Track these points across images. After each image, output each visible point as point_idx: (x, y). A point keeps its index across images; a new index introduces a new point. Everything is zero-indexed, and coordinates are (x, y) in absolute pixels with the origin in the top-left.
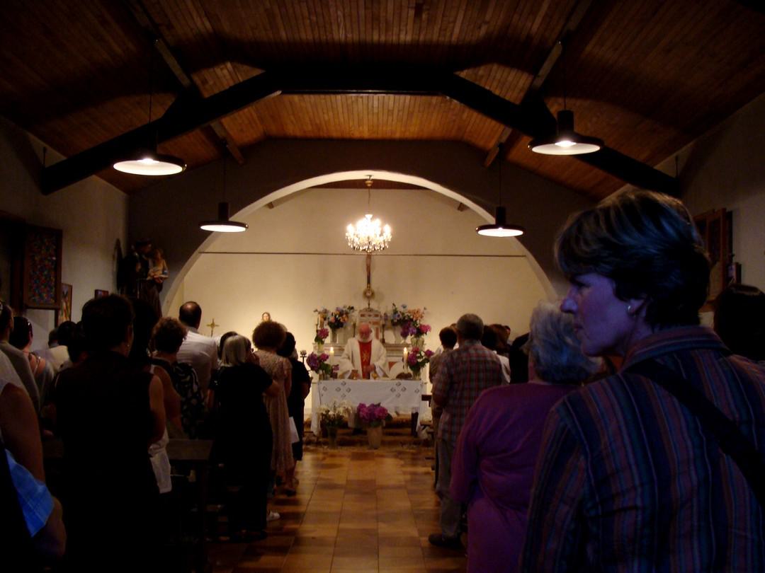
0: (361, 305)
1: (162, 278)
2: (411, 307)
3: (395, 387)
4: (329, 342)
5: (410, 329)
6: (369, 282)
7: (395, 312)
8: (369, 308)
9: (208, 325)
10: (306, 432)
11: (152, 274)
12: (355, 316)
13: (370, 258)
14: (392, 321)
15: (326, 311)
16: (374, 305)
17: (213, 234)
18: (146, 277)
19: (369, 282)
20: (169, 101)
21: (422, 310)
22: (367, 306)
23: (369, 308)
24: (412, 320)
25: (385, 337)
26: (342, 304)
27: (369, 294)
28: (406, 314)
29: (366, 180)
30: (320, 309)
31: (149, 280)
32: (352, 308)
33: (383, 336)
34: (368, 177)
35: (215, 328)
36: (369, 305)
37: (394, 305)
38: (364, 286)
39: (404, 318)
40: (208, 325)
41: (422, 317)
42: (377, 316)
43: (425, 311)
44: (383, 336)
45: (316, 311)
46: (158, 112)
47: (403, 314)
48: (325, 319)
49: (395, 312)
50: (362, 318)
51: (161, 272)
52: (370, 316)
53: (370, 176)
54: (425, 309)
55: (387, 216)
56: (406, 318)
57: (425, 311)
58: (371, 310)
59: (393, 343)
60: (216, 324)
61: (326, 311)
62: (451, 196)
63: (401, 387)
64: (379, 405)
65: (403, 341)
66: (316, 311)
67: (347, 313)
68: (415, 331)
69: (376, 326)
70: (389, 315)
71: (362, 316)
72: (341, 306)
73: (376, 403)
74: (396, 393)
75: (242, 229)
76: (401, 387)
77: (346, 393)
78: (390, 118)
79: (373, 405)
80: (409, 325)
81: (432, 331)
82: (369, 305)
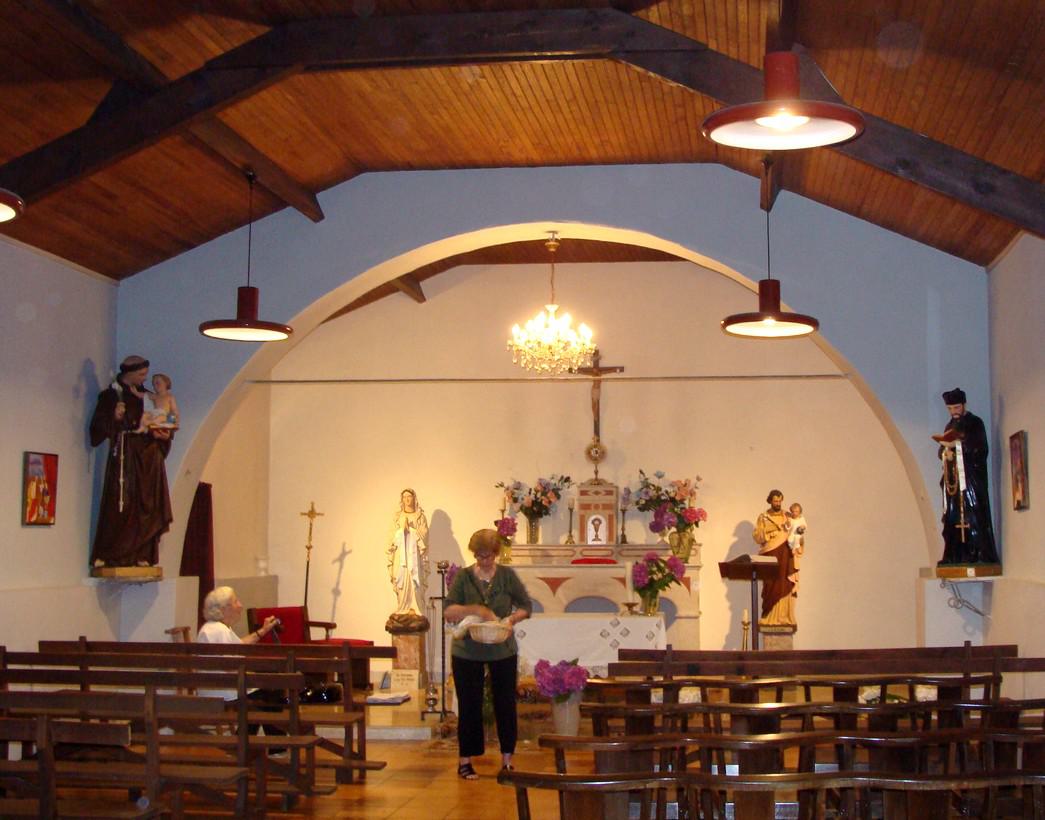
0: (582, 473)
1: (165, 430)
2: (671, 476)
3: (609, 629)
4: (524, 542)
5: (666, 517)
6: (597, 431)
7: (646, 485)
8: (596, 479)
9: (303, 514)
10: (526, 716)
11: (148, 423)
12: (571, 493)
13: (599, 387)
14: (637, 503)
15: (518, 486)
16: (606, 473)
17: (263, 347)
18: (137, 427)
19: (597, 431)
20: (101, 90)
21: (694, 481)
22: (594, 477)
23: (596, 479)
24: (673, 500)
25: (626, 533)
26: (549, 472)
27: (596, 454)
28: (663, 491)
29: (547, 240)
30: (509, 483)
31: (142, 434)
32: (567, 479)
33: (623, 529)
34: (550, 236)
35: (317, 520)
36: (596, 472)
37: (641, 472)
38: (588, 438)
39: (659, 497)
40: (303, 514)
41: (692, 494)
42: (609, 493)
43: (699, 484)
44: (623, 529)
45: (502, 485)
46: (84, 114)
47: (658, 489)
48: (515, 500)
49: (646, 485)
50: (583, 497)
51: (165, 419)
52: (597, 493)
53: (554, 232)
54: (698, 479)
55: (584, 305)
56: (663, 498)
57: (699, 484)
58: (597, 482)
59: (643, 542)
60: (317, 511)
61: (518, 486)
62: (405, 256)
63: (620, 628)
64: (575, 662)
65: (659, 539)
66: (502, 485)
67: (556, 492)
68: (675, 520)
69: (608, 512)
70: (633, 490)
71: (583, 493)
72: (547, 477)
73: (569, 659)
74: (610, 640)
75: (281, 336)
76: (620, 628)
77: (610, 640)
78: (560, 117)
79: (564, 664)
80: (665, 508)
81: (709, 518)
82: (596, 472)
